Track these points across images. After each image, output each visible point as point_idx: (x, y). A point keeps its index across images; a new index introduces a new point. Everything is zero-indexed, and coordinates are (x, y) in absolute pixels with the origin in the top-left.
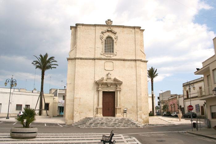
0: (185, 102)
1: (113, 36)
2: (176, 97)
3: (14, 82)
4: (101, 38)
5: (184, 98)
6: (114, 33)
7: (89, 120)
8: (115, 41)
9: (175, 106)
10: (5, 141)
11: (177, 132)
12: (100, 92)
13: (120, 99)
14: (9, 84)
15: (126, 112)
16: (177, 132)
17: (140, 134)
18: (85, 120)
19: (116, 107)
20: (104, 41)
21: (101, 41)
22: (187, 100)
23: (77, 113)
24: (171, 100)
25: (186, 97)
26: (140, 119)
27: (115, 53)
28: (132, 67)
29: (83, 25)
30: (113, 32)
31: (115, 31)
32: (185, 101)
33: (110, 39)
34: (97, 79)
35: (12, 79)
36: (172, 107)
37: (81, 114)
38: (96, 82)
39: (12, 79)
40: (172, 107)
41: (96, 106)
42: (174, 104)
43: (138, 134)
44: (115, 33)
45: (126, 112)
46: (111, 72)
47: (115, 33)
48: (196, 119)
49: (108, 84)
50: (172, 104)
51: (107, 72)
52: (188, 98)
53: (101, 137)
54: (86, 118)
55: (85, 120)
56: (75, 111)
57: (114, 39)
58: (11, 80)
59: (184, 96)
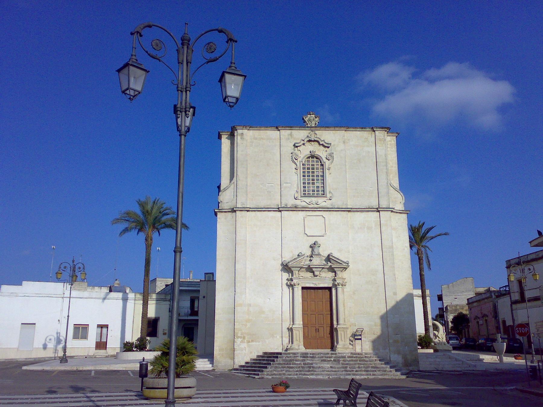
0: (516, 309)
1: (322, 152)
2: (488, 295)
3: (80, 268)
4: (294, 160)
5: (513, 299)
6: (325, 147)
7: (275, 359)
8: (327, 163)
9: (486, 320)
10: (117, 400)
11: (492, 388)
12: (296, 289)
13: (344, 306)
14: (66, 274)
15: (361, 339)
16: (492, 388)
17: (401, 391)
18: (264, 360)
19: (335, 326)
20: (302, 166)
21: (294, 166)
22: (519, 306)
23: (242, 342)
24: (475, 304)
25: (516, 296)
26: (396, 356)
27: (328, 195)
28: (369, 228)
29: (108, 330)
30: (322, 145)
31: (326, 141)
32: (514, 306)
33: (315, 159)
34: (287, 257)
35: (73, 261)
36: (478, 322)
37: (253, 343)
38: (287, 265)
39: (73, 261)
40: (481, 322)
41: (287, 324)
42: (484, 316)
43: (399, 391)
44: (326, 146)
45: (361, 339)
46: (320, 240)
47: (326, 146)
48: (523, 356)
49: (314, 269)
50: (480, 316)
51: (312, 241)
52: (523, 299)
53: (365, 398)
54: (265, 353)
55: (264, 360)
56: (238, 337)
57: (325, 160)
58: (72, 265)
59: (512, 294)
